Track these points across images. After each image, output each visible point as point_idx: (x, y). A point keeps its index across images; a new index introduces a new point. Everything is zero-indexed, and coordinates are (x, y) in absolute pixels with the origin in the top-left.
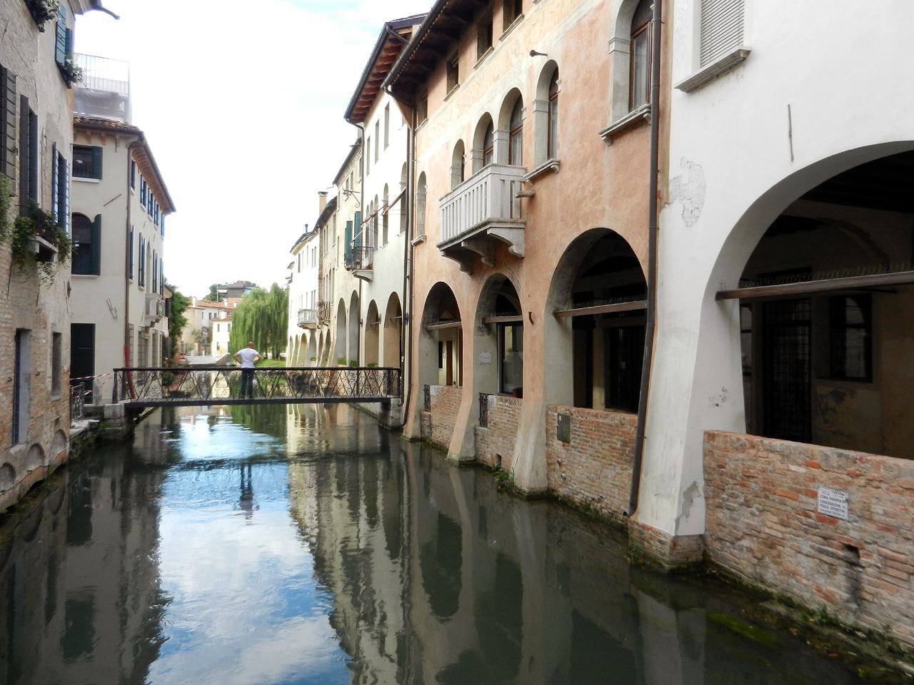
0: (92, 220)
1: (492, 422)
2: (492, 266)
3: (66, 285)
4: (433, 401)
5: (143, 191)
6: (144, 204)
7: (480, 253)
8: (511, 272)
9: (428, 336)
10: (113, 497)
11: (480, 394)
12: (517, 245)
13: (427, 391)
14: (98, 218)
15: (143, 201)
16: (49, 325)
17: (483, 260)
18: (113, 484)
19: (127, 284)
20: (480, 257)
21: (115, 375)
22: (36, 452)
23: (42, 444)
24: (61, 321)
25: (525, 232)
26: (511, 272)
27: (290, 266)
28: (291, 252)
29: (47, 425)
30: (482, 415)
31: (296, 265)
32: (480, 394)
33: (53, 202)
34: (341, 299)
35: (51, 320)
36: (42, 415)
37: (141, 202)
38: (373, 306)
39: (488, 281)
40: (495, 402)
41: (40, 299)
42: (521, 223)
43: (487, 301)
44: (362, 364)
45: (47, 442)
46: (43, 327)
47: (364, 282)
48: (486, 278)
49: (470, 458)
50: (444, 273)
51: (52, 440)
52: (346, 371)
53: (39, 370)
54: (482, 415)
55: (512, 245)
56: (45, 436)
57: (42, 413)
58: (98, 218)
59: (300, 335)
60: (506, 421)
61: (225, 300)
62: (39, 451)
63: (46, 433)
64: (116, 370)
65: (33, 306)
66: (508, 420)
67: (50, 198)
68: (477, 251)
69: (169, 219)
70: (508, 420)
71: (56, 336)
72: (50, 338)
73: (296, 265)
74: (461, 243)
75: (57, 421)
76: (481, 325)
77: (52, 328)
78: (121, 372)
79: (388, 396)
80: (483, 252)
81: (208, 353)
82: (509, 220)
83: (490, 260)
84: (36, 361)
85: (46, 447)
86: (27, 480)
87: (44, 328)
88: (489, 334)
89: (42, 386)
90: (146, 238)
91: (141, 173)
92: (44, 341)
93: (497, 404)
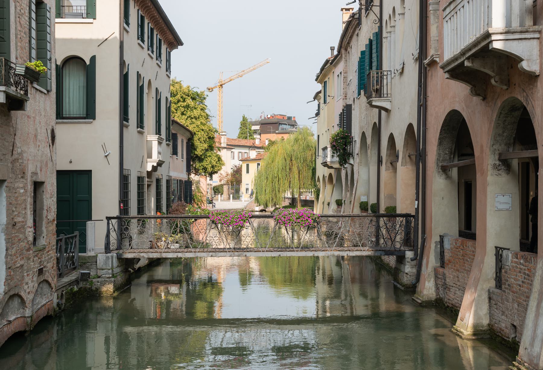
0: (88, 63)
1: (507, 283)
2: (505, 87)
3: (49, 132)
4: (447, 255)
5: (141, 26)
6: (143, 41)
7: (487, 71)
8: (525, 94)
9: (444, 176)
10: (108, 352)
11: (496, 248)
12: (528, 60)
13: (442, 242)
14: (93, 59)
15: (141, 37)
16: (29, 175)
17: (493, 81)
18: (107, 340)
19: (122, 127)
20: (490, 77)
21: (108, 224)
22: (16, 303)
23: (22, 294)
24: (44, 170)
25: (540, 43)
26: (525, 94)
27: (316, 97)
28: (316, 80)
29: (28, 275)
30: (498, 274)
31: (322, 95)
32: (496, 248)
33: (30, 48)
34: (364, 132)
35: (31, 168)
36: (22, 266)
37: (138, 39)
38: (391, 138)
39: (502, 108)
40: (510, 258)
41: (15, 149)
42: (534, 32)
43: (503, 132)
44: (382, 211)
45: (29, 293)
46: (20, 176)
47: (383, 113)
48: (499, 103)
49: (483, 326)
50: (457, 100)
51: (34, 290)
52: (385, 218)
53: (15, 220)
54: (498, 274)
55: (522, 60)
56: (26, 287)
57: (22, 262)
58: (93, 59)
59: (327, 175)
60: (520, 283)
61: (256, 136)
62: (20, 301)
63: (27, 284)
64: (108, 219)
65: (8, 157)
66: (523, 282)
67: (27, 45)
68: (482, 70)
69: (174, 53)
70: (523, 282)
71: (38, 185)
72: (30, 188)
73: (322, 95)
74: (463, 63)
75: (41, 272)
76: (498, 163)
77: (32, 177)
78: (114, 221)
79: (402, 248)
80: (493, 71)
81: (236, 195)
82: (519, 29)
83: (502, 82)
84: (13, 211)
85: (28, 298)
86: (5, 329)
87: (22, 177)
88: (508, 174)
89: (21, 236)
90: (147, 76)
91: (137, 8)
92: (22, 191)
93: (512, 262)
